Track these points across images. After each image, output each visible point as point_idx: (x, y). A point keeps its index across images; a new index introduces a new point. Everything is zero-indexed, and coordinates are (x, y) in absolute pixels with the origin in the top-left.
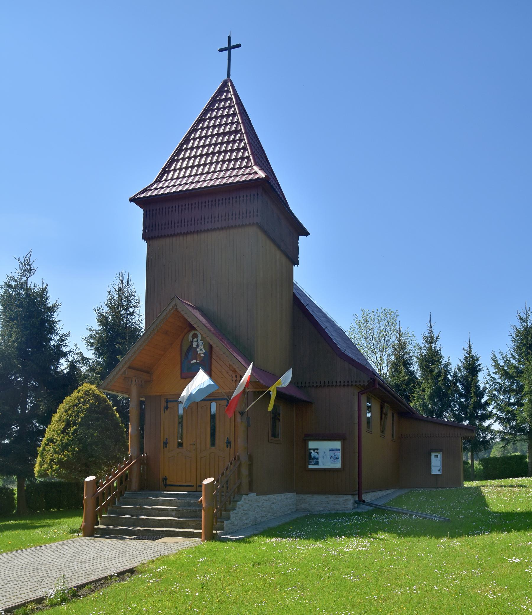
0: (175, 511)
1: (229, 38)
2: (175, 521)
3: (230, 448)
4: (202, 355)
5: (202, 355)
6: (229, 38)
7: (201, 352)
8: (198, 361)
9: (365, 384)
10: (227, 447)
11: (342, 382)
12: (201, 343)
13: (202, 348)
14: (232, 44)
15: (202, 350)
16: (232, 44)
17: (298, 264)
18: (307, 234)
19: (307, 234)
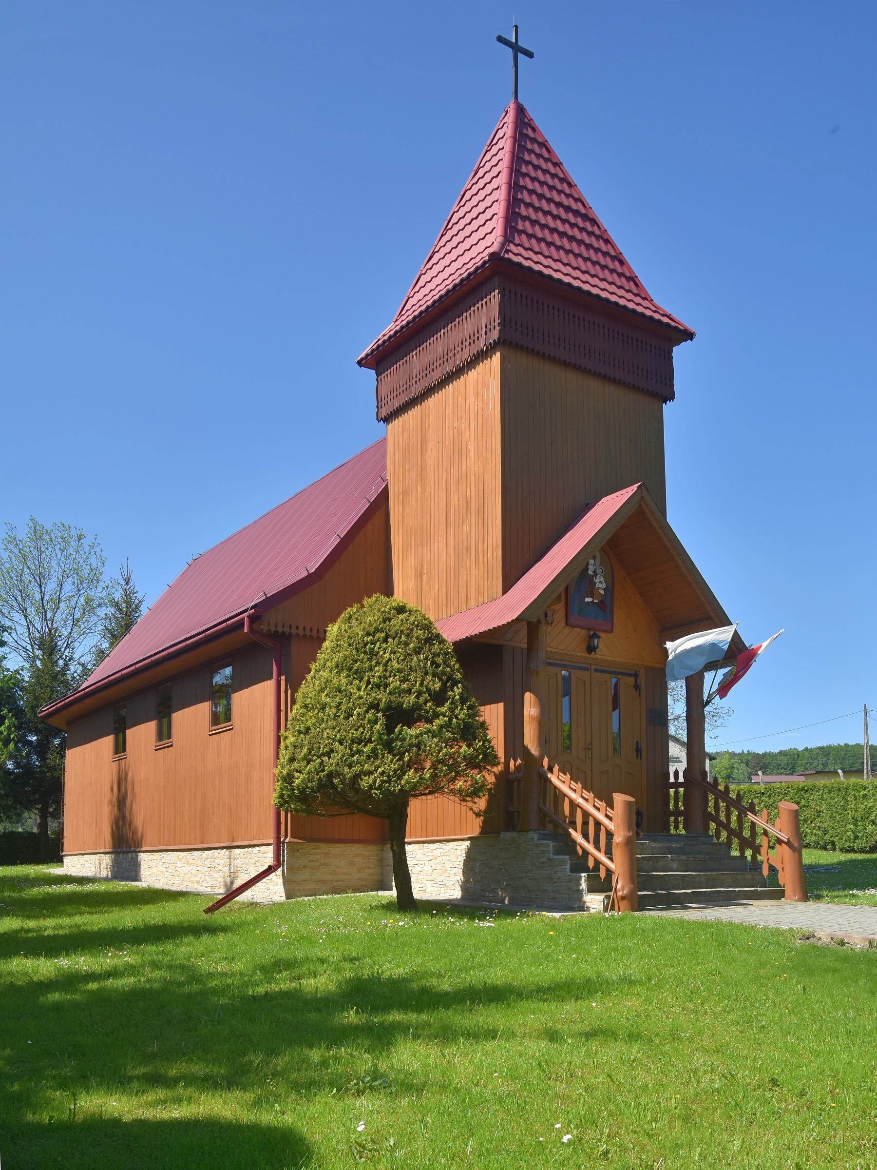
0: (676, 862)
1: (500, 39)
2: (704, 877)
3: (641, 759)
4: (602, 592)
5: (602, 592)
6: (500, 39)
7: (600, 585)
8: (595, 601)
9: (278, 629)
10: (637, 757)
11: (308, 630)
12: (600, 570)
13: (602, 579)
14: (520, 55)
15: (601, 582)
16: (520, 55)
17: (671, 397)
18: (688, 335)
19: (688, 335)
